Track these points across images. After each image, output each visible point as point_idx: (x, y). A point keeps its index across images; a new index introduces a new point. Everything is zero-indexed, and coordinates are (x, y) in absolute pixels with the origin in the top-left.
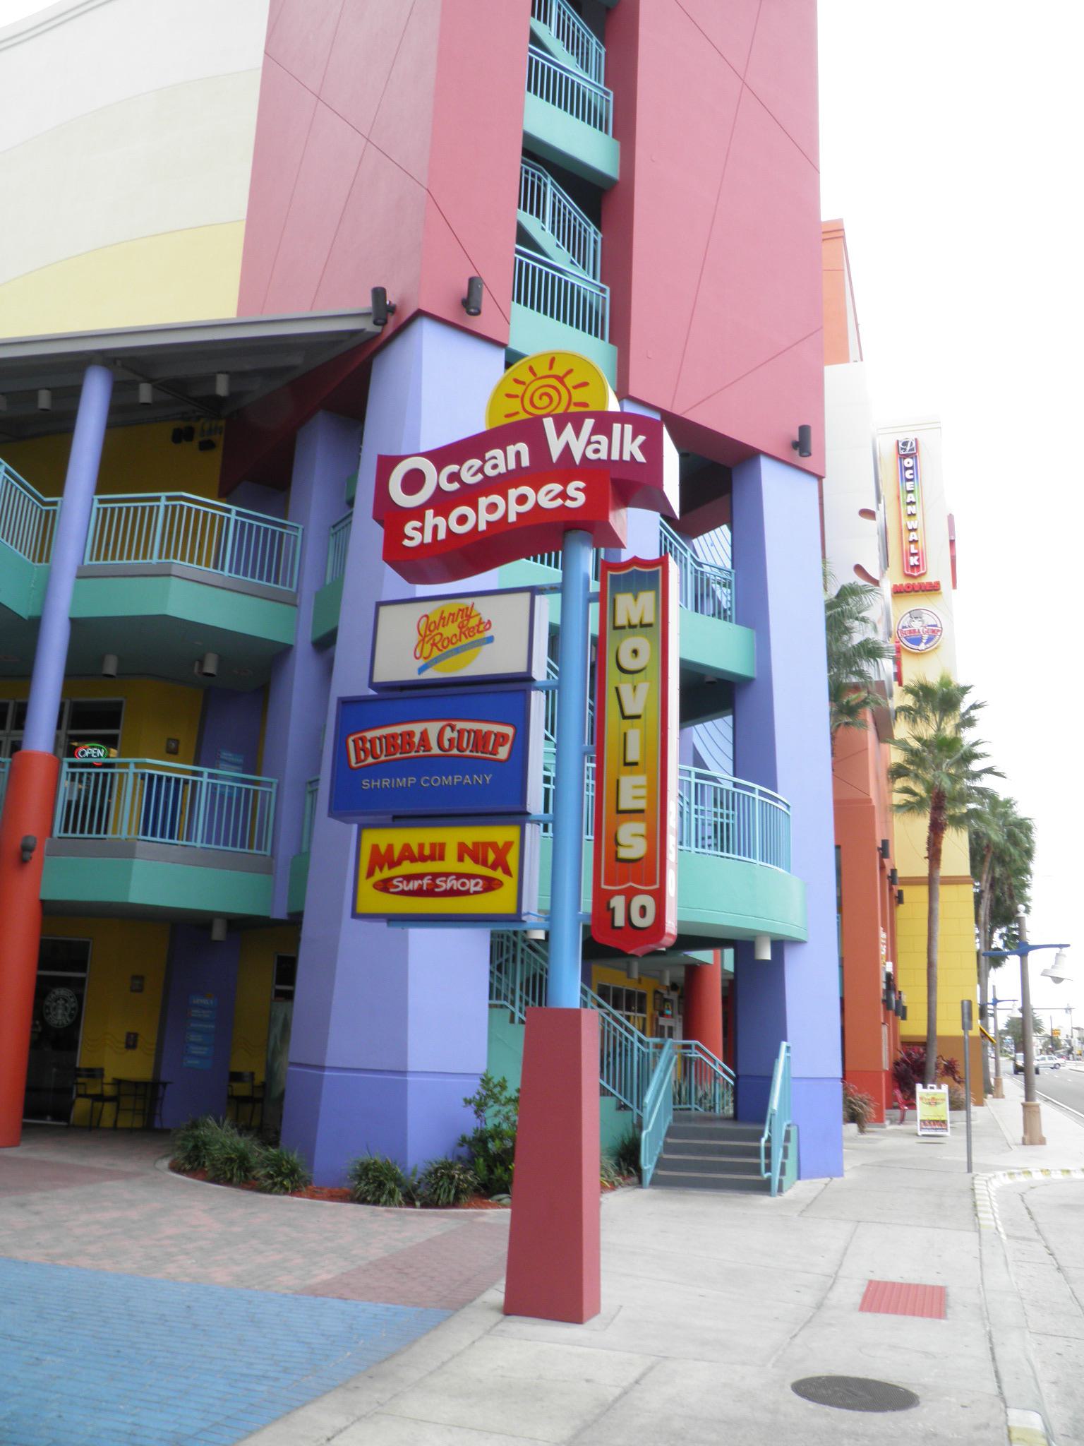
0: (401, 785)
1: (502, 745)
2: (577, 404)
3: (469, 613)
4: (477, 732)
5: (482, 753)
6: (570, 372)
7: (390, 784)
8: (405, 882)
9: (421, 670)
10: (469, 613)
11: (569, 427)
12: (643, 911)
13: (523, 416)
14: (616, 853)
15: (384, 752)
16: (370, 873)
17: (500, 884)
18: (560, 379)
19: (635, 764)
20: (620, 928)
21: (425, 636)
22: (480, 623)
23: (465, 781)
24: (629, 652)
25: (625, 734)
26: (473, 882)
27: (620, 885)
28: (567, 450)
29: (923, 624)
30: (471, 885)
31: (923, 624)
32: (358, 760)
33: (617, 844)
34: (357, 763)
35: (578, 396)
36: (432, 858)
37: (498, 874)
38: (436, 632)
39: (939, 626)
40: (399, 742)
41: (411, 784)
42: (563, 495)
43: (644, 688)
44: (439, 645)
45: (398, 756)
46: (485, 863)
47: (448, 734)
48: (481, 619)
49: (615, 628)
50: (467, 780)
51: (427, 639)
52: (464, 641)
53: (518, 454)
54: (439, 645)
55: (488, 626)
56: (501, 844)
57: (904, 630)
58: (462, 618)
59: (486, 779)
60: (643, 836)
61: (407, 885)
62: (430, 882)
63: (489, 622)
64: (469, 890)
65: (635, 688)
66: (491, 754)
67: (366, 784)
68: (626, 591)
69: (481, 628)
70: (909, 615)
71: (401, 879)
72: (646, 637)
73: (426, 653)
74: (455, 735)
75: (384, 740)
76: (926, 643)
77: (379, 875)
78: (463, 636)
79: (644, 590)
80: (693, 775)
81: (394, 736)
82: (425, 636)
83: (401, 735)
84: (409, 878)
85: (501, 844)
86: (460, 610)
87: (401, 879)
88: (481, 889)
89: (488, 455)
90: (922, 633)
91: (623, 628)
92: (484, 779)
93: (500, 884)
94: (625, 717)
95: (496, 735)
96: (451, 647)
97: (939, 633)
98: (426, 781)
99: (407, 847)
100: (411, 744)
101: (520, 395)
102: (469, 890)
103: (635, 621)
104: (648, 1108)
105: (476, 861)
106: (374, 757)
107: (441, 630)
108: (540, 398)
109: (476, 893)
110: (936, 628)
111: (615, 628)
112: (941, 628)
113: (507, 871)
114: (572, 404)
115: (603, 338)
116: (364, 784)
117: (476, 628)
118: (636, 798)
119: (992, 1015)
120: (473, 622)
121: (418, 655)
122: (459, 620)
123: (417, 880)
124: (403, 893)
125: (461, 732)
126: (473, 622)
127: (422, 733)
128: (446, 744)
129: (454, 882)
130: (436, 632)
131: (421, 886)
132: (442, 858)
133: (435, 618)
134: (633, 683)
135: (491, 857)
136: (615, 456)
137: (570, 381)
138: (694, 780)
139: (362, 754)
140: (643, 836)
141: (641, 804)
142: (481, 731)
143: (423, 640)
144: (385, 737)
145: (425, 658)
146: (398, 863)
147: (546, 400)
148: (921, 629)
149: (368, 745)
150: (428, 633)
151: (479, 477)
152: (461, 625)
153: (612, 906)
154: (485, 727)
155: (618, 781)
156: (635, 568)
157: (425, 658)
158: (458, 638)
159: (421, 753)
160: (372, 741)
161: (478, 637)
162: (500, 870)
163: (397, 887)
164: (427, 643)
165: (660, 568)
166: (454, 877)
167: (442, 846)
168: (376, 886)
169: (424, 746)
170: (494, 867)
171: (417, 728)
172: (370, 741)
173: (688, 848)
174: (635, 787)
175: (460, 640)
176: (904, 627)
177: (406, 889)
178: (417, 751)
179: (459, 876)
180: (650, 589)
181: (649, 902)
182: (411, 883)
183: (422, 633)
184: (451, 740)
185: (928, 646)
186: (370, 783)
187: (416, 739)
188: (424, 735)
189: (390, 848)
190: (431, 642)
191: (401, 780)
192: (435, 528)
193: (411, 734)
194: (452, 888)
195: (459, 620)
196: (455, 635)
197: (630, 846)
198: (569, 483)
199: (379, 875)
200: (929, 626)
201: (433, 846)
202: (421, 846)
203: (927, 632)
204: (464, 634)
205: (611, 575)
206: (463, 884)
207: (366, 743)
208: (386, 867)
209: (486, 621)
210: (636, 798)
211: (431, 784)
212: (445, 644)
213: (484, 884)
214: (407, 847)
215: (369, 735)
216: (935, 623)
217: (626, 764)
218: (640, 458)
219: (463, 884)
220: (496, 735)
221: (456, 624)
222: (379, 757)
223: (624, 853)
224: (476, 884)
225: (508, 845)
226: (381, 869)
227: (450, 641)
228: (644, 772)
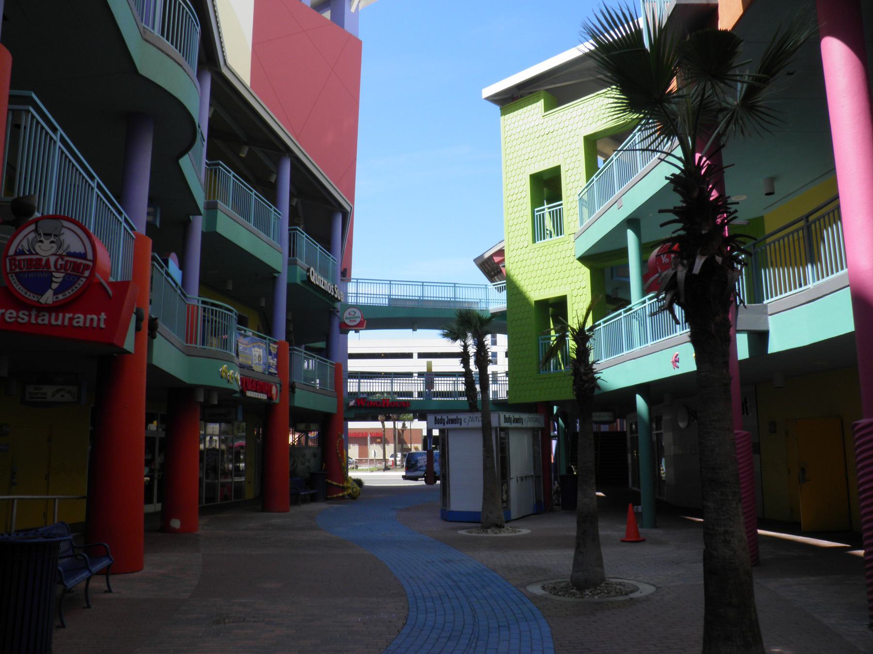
0: (42, 276)
4: (75, 263)
5: (77, 272)
29: (59, 248)
31: (59, 248)
39: (90, 256)
47: (60, 262)
57: (18, 258)
66: (81, 273)
80: (200, 302)
90: (53, 269)
104: (275, 396)
115: (561, 205)
119: (429, 384)
125: (67, 262)
128: (59, 267)
138: (200, 305)
139: (13, 267)
149: (17, 263)
159: (45, 269)
160: (20, 261)
173: (195, 346)
178: (43, 268)
184: (61, 265)
187: (43, 263)
200: (70, 254)
216: (83, 251)
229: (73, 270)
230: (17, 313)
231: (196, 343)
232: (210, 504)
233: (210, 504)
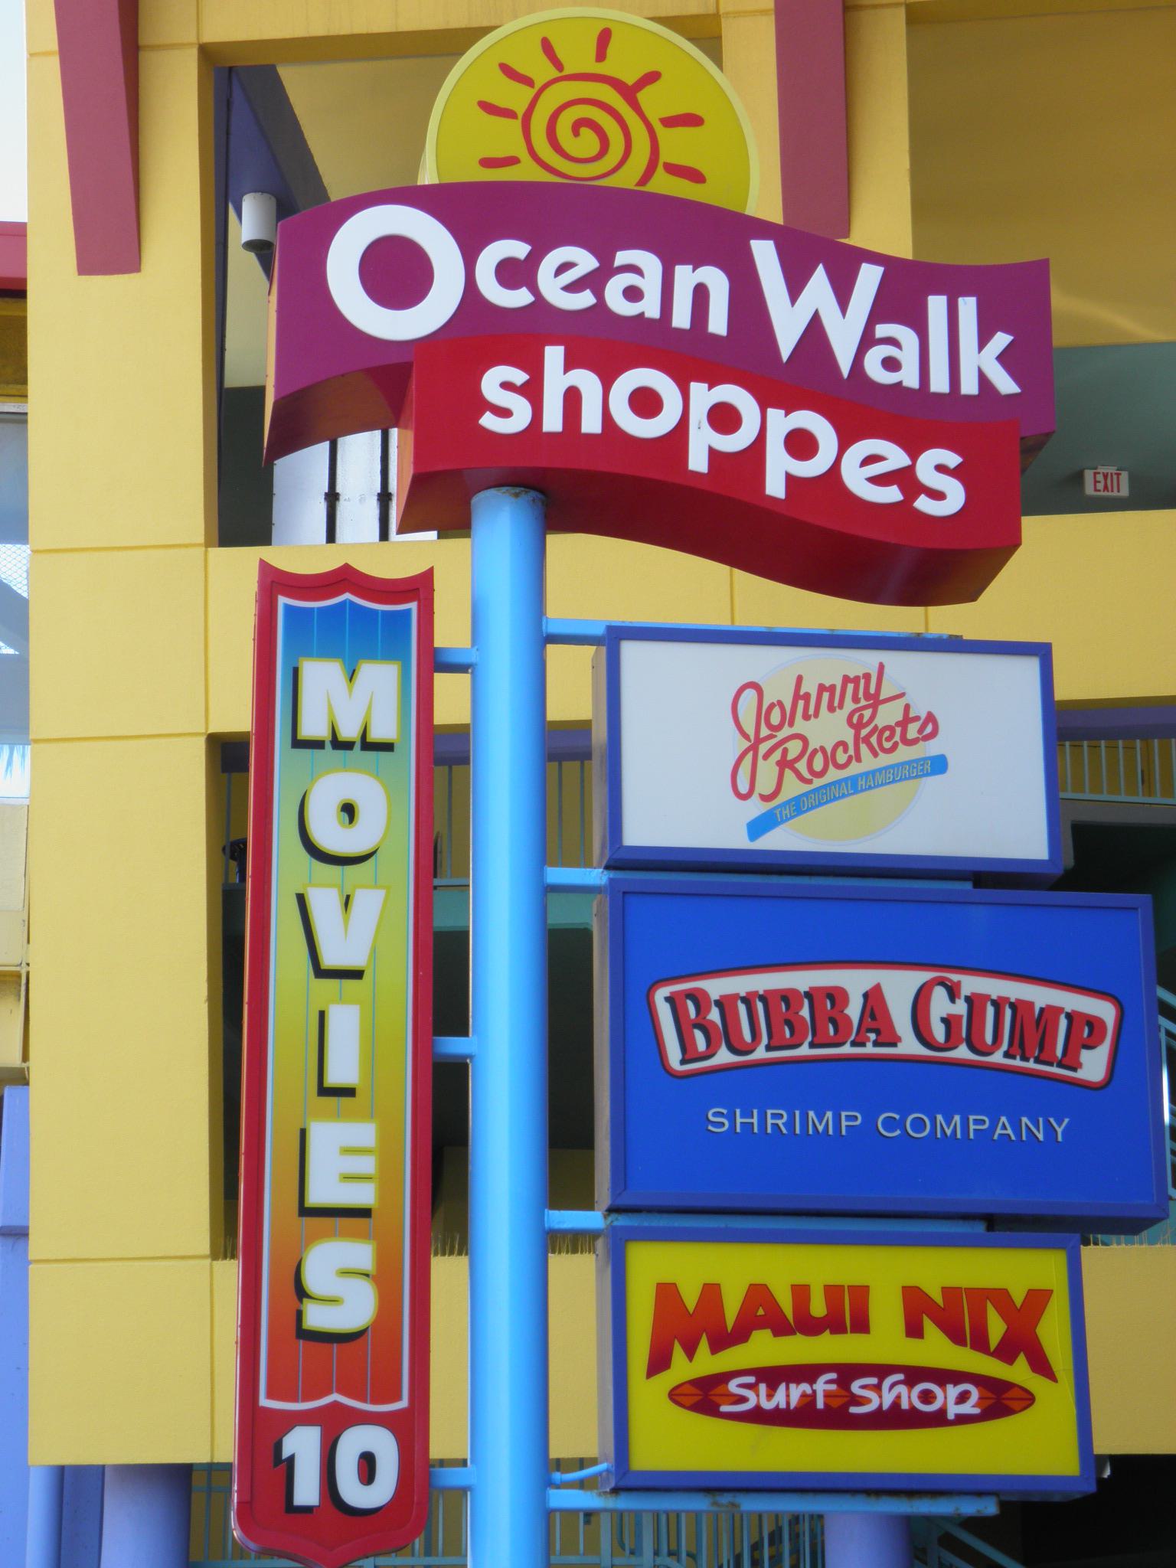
1: (1089, 1047)
2: (673, 169)
3: (872, 690)
4: (1019, 1008)
5: (1038, 1061)
6: (652, 77)
7: (790, 1124)
8: (763, 1388)
9: (757, 828)
10: (872, 690)
11: (820, 275)
12: (367, 1466)
13: (527, 172)
14: (299, 1315)
15: (1005, 1046)
16: (659, 1363)
17: (1027, 1399)
18: (629, 93)
19: (349, 1092)
20: (307, 1510)
21: (759, 741)
22: (907, 720)
23: (999, 1131)
24: (335, 805)
25: (322, 1015)
26: (953, 1391)
27: (305, 1399)
28: (815, 329)
30: (947, 1397)
32: (688, 1053)
33: (301, 1293)
34: (683, 1062)
35: (676, 146)
36: (833, 1324)
37: (1019, 1372)
38: (786, 732)
40: (805, 1012)
42: (905, 479)
43: (369, 903)
44: (802, 766)
45: (804, 1050)
46: (980, 1343)
47: (940, 1005)
48: (907, 708)
49: (298, 743)
50: (1004, 1127)
51: (763, 748)
52: (869, 761)
53: (701, 294)
54: (802, 766)
55: (929, 729)
56: (1018, 1298)
58: (856, 699)
59: (1056, 1131)
60: (367, 1275)
61: (770, 1396)
62: (833, 1387)
63: (931, 718)
64: (943, 1410)
65: (347, 902)
66: (1060, 1065)
67: (725, 1111)
68: (326, 652)
69: (912, 731)
71: (751, 1379)
72: (377, 775)
73: (767, 784)
74: (960, 1008)
75: (760, 1006)
77: (683, 1369)
78: (864, 749)
79: (372, 657)
81: (788, 997)
82: (759, 741)
83: (808, 995)
84: (772, 1376)
85: (1018, 1298)
86: (846, 679)
87: (751, 1379)
88: (977, 1411)
89: (622, 257)
91: (318, 744)
92: (1050, 1131)
93: (1027, 1399)
94: (321, 973)
96: (833, 774)
98: (889, 1124)
99: (758, 1294)
100: (839, 1022)
101: (520, 112)
102: (943, 1410)
103: (349, 731)
105: (956, 1336)
106: (733, 1049)
107: (800, 726)
108: (577, 126)
109: (962, 1420)
111: (298, 743)
113: (1041, 1366)
114: (660, 169)
116: (711, 1118)
117: (898, 730)
118: (348, 1178)
120: (889, 715)
121: (743, 788)
122: (849, 705)
123: (798, 1382)
124: (757, 1416)
125: (975, 1003)
126: (889, 715)
127: (866, 996)
128: (939, 1032)
129: (902, 1389)
130: (786, 732)
131: (809, 1400)
132: (861, 1325)
133: (780, 691)
134: (342, 889)
135: (996, 1328)
136: (939, 383)
137: (656, 102)
140: (367, 1275)
141: (363, 1195)
142: (1030, 1005)
143: (754, 748)
144: (763, 998)
145: (765, 798)
146: (740, 1335)
147: (588, 144)
149: (714, 1015)
150: (765, 732)
151: (585, 299)
152: (855, 720)
153: (286, 1454)
154: (1040, 996)
155: (303, 1133)
156: (347, 596)
157: (765, 798)
158: (851, 752)
159: (869, 1049)
160: (725, 1004)
161: (904, 753)
162: (1022, 1361)
163: (743, 1400)
164: (766, 757)
165: (413, 606)
166: (900, 1377)
167: (860, 1294)
168: (676, 1395)
169: (878, 1032)
170: (1006, 1353)
171: (855, 982)
172: (718, 1003)
174: (347, 1151)
175: (859, 759)
177: (767, 1405)
179: (913, 1375)
180: (388, 656)
181: (383, 1444)
182: (782, 1389)
183: (750, 731)
184: (948, 1022)
186: (732, 1119)
187: (854, 1010)
188: (874, 999)
189: (711, 1293)
190: (777, 755)
191: (820, 1118)
192: (572, 398)
193: (838, 997)
194: (896, 1404)
195: (849, 705)
196: (843, 744)
197: (333, 1301)
199: (683, 1369)
201: (833, 1293)
202: (801, 1293)
204: (866, 740)
205: (287, 607)
206: (927, 1397)
207: (708, 1011)
208: (704, 1345)
209: (923, 716)
210: (348, 1178)
212: (818, 764)
213: (980, 1398)
214: (758, 1294)
215: (716, 987)
217: (324, 1091)
218: (1005, 384)
219: (927, 1397)
221: (842, 715)
223: (317, 1318)
224: (963, 1398)
225: (1038, 1299)
226: (690, 1352)
227: (830, 760)
228: (371, 1115)
230: (845, 443)
231: (1112, 491)
232: (1121, 763)
233: (1121, 763)
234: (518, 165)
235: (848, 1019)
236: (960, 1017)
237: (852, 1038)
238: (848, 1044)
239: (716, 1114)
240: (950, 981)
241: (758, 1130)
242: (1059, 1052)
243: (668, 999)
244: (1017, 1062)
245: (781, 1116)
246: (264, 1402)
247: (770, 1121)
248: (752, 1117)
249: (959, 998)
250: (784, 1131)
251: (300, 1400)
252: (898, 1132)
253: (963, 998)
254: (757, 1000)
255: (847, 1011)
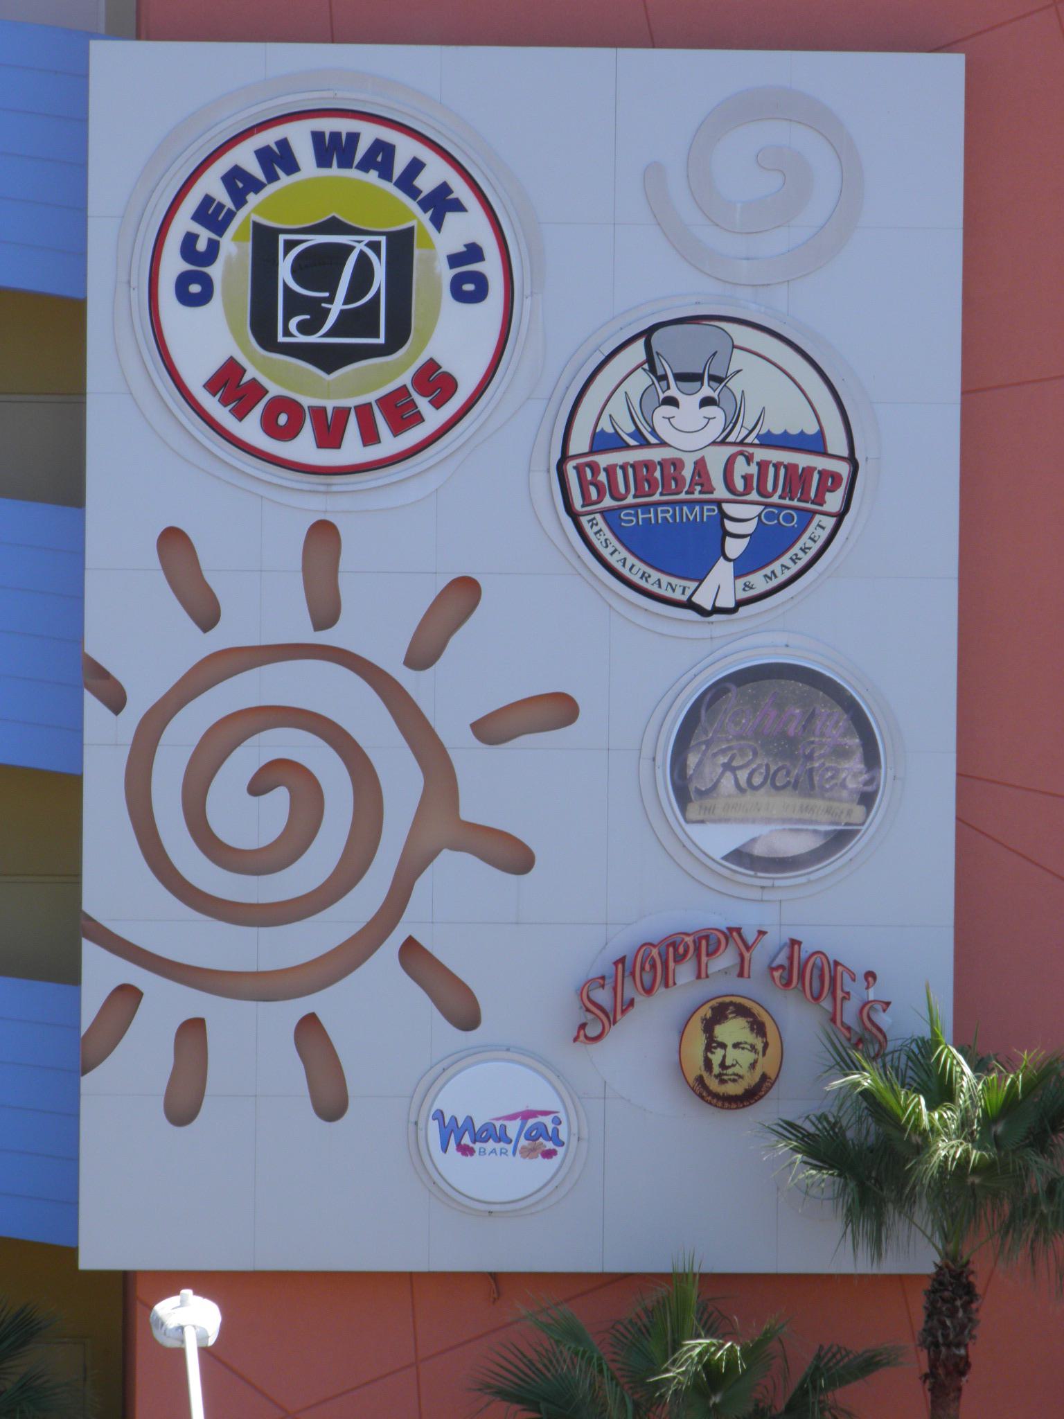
0: (691, 518)
1: (832, 490)
4: (791, 468)
7: (674, 516)
34: (583, 506)
39: (836, 443)
40: (658, 474)
41: (708, 516)
45: (656, 497)
47: (741, 467)
57: (603, 460)
66: (813, 502)
70: (637, 352)
74: (753, 469)
75: (630, 471)
76: (743, 567)
81: (648, 465)
83: (660, 463)
95: (820, 472)
97: (834, 501)
100: (679, 480)
106: (613, 497)
110: (820, 463)
112: (852, 460)
125: (763, 466)
127: (696, 463)
128: (739, 485)
142: (796, 466)
144: (633, 466)
148: (716, 461)
149: (602, 477)
160: (610, 471)
169: (702, 485)
172: (606, 470)
176: (604, 442)
185: (759, 582)
186: (636, 515)
187: (687, 473)
198: (292, 318)
200: (768, 441)
203: (756, 483)
211: (778, 520)
220: (820, 472)
222: (624, 498)
229: (788, 492)
234: (425, 168)
235: (684, 479)
236: (752, 476)
237: (686, 489)
238: (684, 493)
239: (626, 515)
240: (747, 452)
241: (642, 522)
242: (812, 495)
243: (575, 468)
244: (787, 502)
245: (668, 512)
246: (381, 340)
247: (660, 515)
248: (650, 513)
249: (753, 462)
250: (671, 521)
251: (411, 398)
252: (776, 522)
253: (755, 463)
254: (629, 467)
255: (684, 473)
